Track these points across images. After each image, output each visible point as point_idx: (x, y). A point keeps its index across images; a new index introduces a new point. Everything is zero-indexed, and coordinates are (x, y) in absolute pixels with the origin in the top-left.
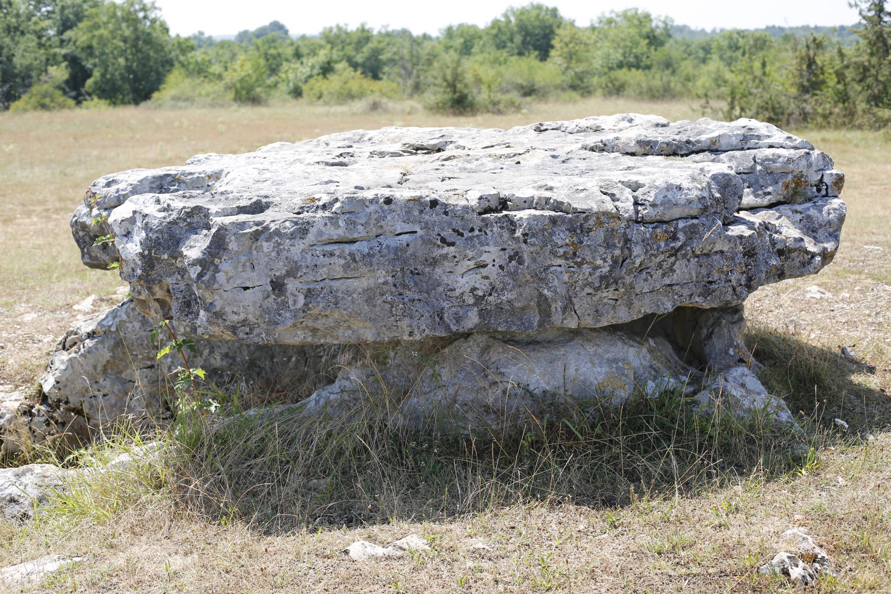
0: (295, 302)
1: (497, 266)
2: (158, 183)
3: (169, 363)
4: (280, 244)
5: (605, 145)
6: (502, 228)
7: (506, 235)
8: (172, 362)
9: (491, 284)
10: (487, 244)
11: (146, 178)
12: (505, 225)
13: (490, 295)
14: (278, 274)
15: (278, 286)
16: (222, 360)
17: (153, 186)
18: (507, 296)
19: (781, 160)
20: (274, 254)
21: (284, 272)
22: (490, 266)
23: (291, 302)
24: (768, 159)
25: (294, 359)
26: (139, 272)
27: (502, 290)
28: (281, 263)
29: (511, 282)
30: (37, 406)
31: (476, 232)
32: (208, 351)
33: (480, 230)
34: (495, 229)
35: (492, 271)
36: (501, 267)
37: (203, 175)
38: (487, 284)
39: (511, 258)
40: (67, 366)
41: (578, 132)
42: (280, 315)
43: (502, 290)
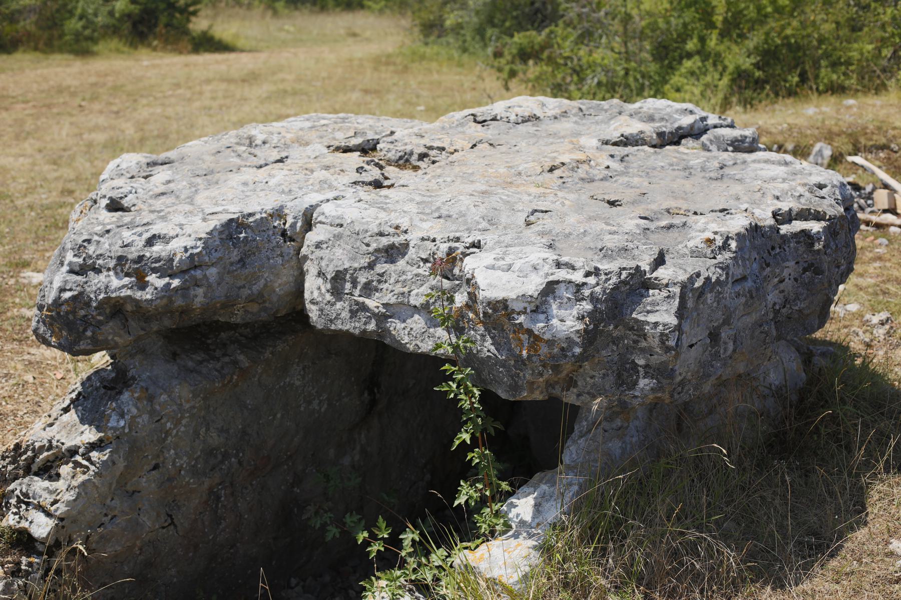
0: (725, 350)
1: (792, 279)
2: (227, 232)
3: (173, 456)
4: (720, 293)
5: (627, 138)
6: (798, 242)
7: (802, 249)
8: (176, 454)
9: (784, 296)
10: (788, 260)
11: (215, 229)
12: (802, 239)
13: (784, 307)
14: (715, 325)
15: (714, 336)
16: (219, 436)
17: (224, 236)
18: (801, 305)
19: (748, 140)
20: (715, 305)
21: (721, 321)
22: (787, 280)
23: (722, 352)
24: (737, 140)
25: (279, 416)
26: (577, 350)
27: (794, 300)
28: (720, 313)
29: (805, 291)
30: (24, 560)
31: (778, 250)
32: (204, 429)
33: (780, 248)
34: (792, 245)
35: (788, 284)
36: (796, 280)
37: (264, 215)
38: (782, 297)
39: (805, 270)
40: (79, 494)
41: (523, 122)
42: (712, 366)
43: (794, 300)
